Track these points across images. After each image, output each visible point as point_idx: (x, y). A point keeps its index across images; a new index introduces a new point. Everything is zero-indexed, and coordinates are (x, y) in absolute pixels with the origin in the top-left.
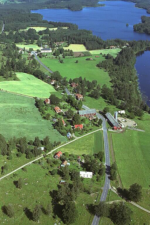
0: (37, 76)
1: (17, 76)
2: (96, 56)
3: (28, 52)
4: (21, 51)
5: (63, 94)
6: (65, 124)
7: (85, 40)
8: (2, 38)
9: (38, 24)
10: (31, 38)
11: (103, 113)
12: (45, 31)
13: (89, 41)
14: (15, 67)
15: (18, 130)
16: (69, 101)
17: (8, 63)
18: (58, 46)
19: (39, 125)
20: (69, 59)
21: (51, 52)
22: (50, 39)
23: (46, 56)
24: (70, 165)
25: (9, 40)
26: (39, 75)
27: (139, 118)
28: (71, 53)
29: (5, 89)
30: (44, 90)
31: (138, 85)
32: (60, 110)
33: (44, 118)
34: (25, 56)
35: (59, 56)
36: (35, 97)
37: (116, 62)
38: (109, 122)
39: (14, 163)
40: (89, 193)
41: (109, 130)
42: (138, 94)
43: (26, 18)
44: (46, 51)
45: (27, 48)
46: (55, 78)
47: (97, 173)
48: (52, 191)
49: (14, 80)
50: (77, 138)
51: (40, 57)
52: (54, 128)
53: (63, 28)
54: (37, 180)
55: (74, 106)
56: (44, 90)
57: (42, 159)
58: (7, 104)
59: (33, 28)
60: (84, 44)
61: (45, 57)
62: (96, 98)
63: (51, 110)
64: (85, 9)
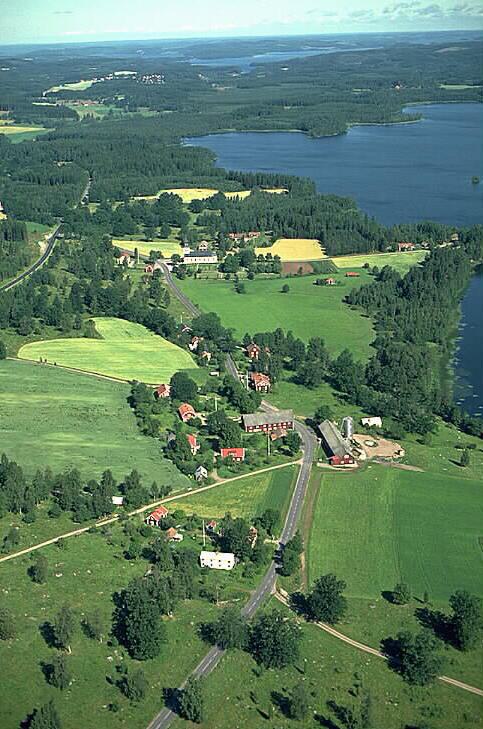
0: (152, 327)
1: (96, 327)
2: (349, 273)
3: (146, 262)
4: (125, 261)
5: (217, 373)
6: (199, 447)
7: (325, 227)
8: (75, 221)
9: (195, 178)
10: (165, 220)
11: (314, 425)
12: (210, 200)
13: (337, 228)
14: (95, 303)
15: (65, 457)
16: (227, 392)
17: (75, 290)
18: (242, 245)
19: (127, 447)
20: (263, 282)
21: (216, 261)
22: (220, 223)
23: (198, 276)
24: (182, 539)
25: (94, 228)
26: (159, 325)
27: (420, 438)
28: (274, 265)
29: (51, 361)
30: (156, 360)
31: (452, 353)
32: (194, 413)
33: (145, 432)
34: (134, 276)
35: (238, 273)
36: (131, 380)
37: (405, 287)
38: (325, 446)
39: (39, 531)
40: (213, 600)
41: (318, 464)
42: (444, 376)
43: (161, 160)
44: (200, 260)
45: (145, 249)
46: (208, 335)
47: (247, 558)
48: (120, 593)
49: (85, 337)
50: (222, 482)
51: (180, 277)
52: (166, 457)
53: (268, 191)
54: (90, 566)
55: (236, 405)
56: (156, 360)
57: (112, 524)
58: (50, 397)
59: (175, 192)
60: (320, 238)
61: (193, 277)
62: (310, 385)
63: (168, 415)
64: (354, 132)
